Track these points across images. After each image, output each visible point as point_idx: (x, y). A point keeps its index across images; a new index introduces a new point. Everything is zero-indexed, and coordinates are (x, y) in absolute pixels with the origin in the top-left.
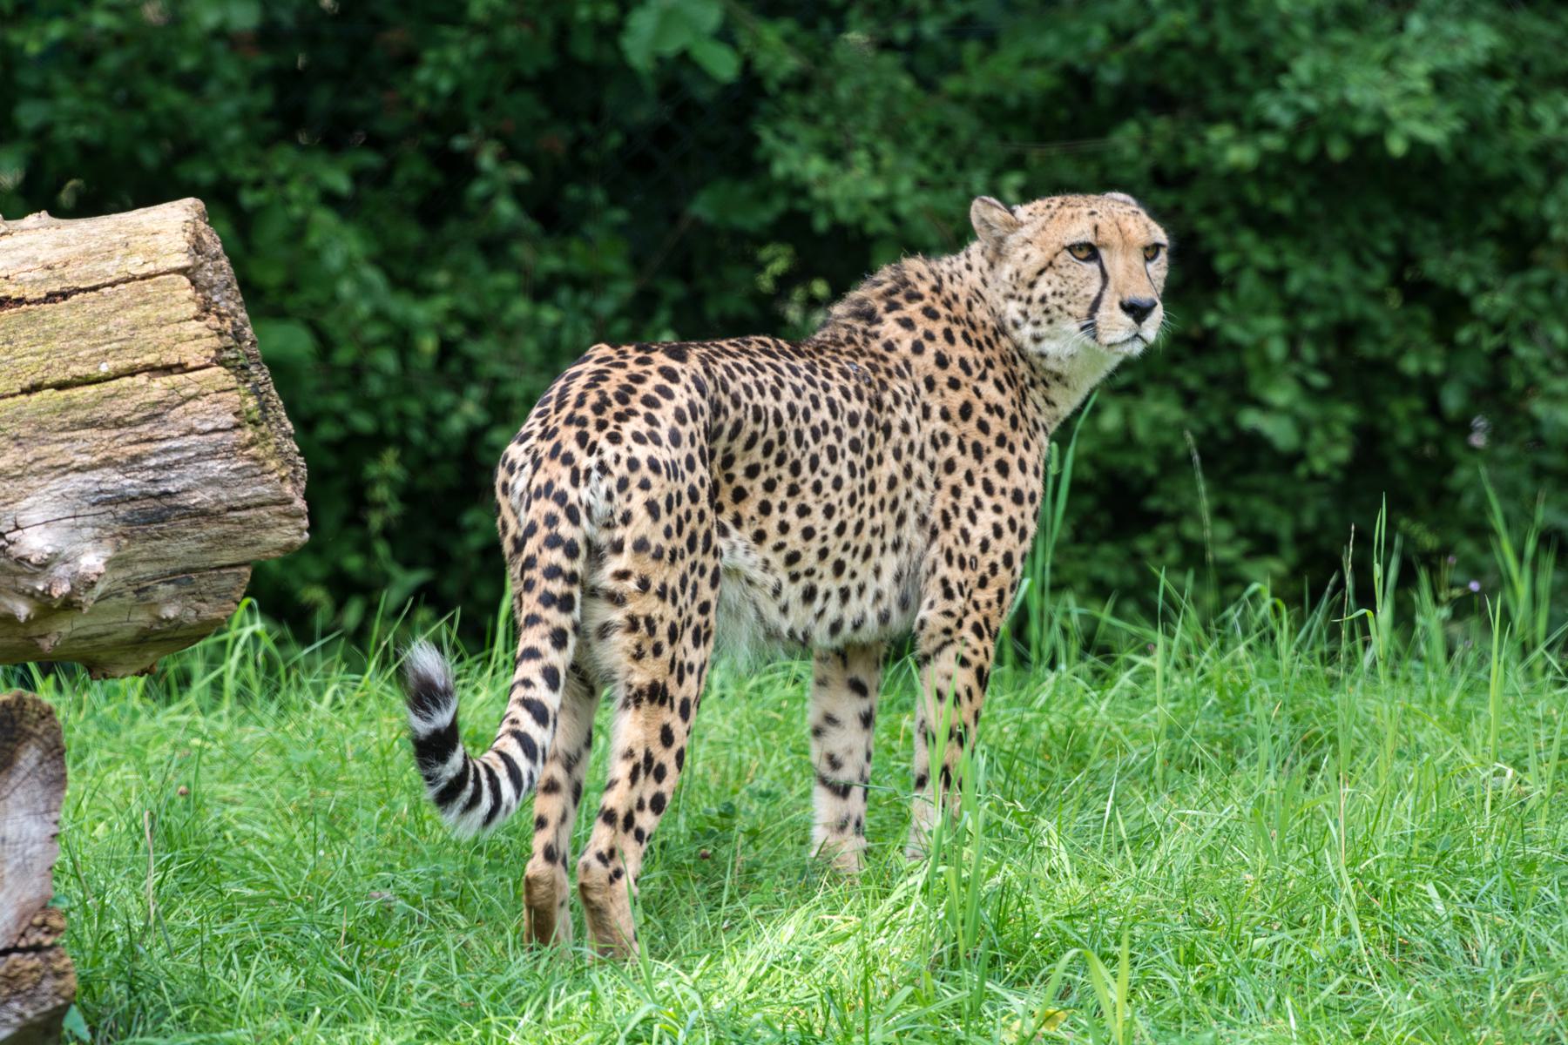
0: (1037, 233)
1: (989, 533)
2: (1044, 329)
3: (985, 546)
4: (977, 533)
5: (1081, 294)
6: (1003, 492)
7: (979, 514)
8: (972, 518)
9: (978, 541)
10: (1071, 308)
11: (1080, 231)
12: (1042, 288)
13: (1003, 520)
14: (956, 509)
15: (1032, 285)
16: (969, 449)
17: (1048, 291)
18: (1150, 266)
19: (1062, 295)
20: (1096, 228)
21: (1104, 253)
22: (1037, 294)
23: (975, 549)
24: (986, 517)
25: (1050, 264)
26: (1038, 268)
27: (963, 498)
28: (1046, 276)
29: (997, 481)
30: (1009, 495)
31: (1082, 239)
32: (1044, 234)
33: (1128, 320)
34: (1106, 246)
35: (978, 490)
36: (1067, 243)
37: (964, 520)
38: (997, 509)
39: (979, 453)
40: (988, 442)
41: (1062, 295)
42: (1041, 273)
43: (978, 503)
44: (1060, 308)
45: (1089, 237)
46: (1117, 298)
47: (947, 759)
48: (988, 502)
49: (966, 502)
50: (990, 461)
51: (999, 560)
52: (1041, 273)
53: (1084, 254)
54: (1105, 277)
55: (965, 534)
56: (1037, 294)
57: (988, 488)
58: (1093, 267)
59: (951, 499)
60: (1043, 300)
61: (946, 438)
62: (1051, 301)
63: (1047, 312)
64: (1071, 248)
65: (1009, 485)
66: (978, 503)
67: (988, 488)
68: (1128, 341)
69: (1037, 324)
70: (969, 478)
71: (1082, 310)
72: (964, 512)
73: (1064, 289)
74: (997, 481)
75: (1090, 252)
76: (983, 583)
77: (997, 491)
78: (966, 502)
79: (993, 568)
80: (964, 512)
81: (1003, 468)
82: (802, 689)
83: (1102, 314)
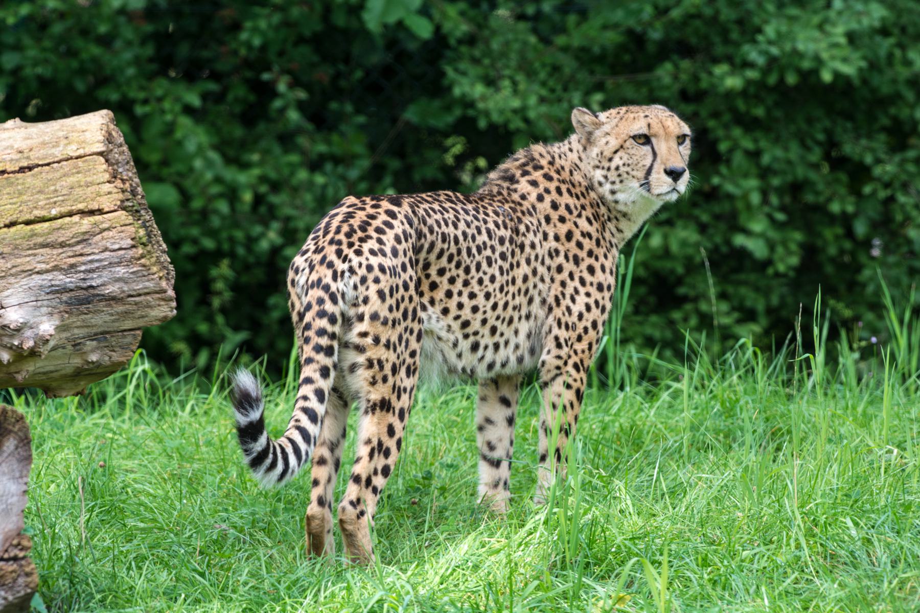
0: (613, 128)
1: (583, 309)
2: (617, 186)
3: (580, 316)
5: (640, 165)
6: (592, 284)
8: (573, 300)
9: (577, 314)
10: (634, 173)
11: (639, 127)
12: (617, 161)
13: (591, 301)
14: (563, 295)
15: (610, 160)
16: (571, 259)
17: (621, 163)
18: (681, 148)
19: (629, 165)
20: (649, 125)
21: (654, 140)
22: (613, 165)
23: (574, 318)
24: (581, 300)
25: (622, 147)
26: (614, 149)
28: (619, 154)
29: (588, 278)
30: (595, 286)
31: (641, 132)
33: (669, 180)
34: (655, 136)
35: (577, 283)
36: (632, 134)
37: (568, 301)
38: (588, 295)
39: (577, 261)
40: (583, 254)
41: (629, 165)
42: (616, 152)
43: (577, 291)
44: (628, 173)
45: (645, 131)
46: (663, 167)
47: (558, 444)
48: (582, 290)
49: (569, 291)
51: (589, 325)
52: (616, 152)
54: (655, 154)
55: (569, 309)
57: (583, 282)
58: (647, 148)
59: (560, 289)
60: (617, 168)
61: (557, 252)
63: (619, 175)
64: (634, 137)
65: (595, 280)
66: (577, 291)
67: (583, 282)
69: (613, 183)
71: (641, 174)
72: (568, 296)
73: (630, 162)
74: (588, 278)
75: (645, 139)
76: (579, 339)
77: (588, 284)
78: (569, 291)
79: (586, 330)
80: (568, 296)
81: (591, 270)
82: (472, 403)
83: (653, 177)
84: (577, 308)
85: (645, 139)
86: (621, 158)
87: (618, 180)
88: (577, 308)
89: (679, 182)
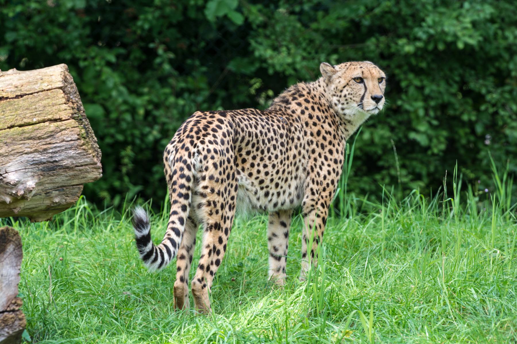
0: (343, 74)
1: (326, 173)
2: (345, 106)
3: (325, 178)
4: (322, 173)
5: (358, 94)
6: (331, 160)
7: (323, 167)
8: (321, 168)
9: (323, 176)
10: (355, 99)
11: (357, 73)
12: (345, 92)
13: (331, 169)
14: (315, 165)
15: (341, 91)
16: (320, 146)
17: (347, 93)
18: (380, 85)
19: (351, 94)
20: (363, 72)
21: (365, 80)
22: (343, 94)
23: (322, 178)
24: (325, 168)
25: (348, 84)
26: (343, 86)
27: (318, 162)
28: (346, 88)
30: (333, 161)
31: (358, 76)
32: (345, 74)
33: (374, 102)
34: (366, 78)
35: (323, 159)
36: (353, 77)
37: (318, 169)
38: (329, 165)
39: (323, 147)
40: (326, 143)
41: (351, 94)
42: (344, 87)
44: (351, 99)
45: (360, 75)
46: (370, 95)
47: (313, 248)
48: (326, 163)
49: (319, 163)
50: (327, 150)
51: (330, 182)
52: (344, 87)
53: (359, 81)
55: (318, 174)
56: (343, 94)
57: (326, 158)
58: (362, 85)
59: (314, 162)
60: (345, 96)
62: (348, 96)
63: (346, 100)
64: (354, 79)
65: (333, 157)
67: (326, 158)
68: (374, 109)
69: (343, 104)
70: (320, 155)
71: (358, 99)
73: (352, 92)
75: (360, 80)
76: (324, 190)
77: (329, 159)
78: (319, 163)
79: (328, 185)
80: (318, 166)
81: (331, 152)
83: (365, 101)
84: (323, 172)
85: (360, 80)
86: (347, 90)
87: (345, 102)
88: (323, 172)
89: (379, 104)
